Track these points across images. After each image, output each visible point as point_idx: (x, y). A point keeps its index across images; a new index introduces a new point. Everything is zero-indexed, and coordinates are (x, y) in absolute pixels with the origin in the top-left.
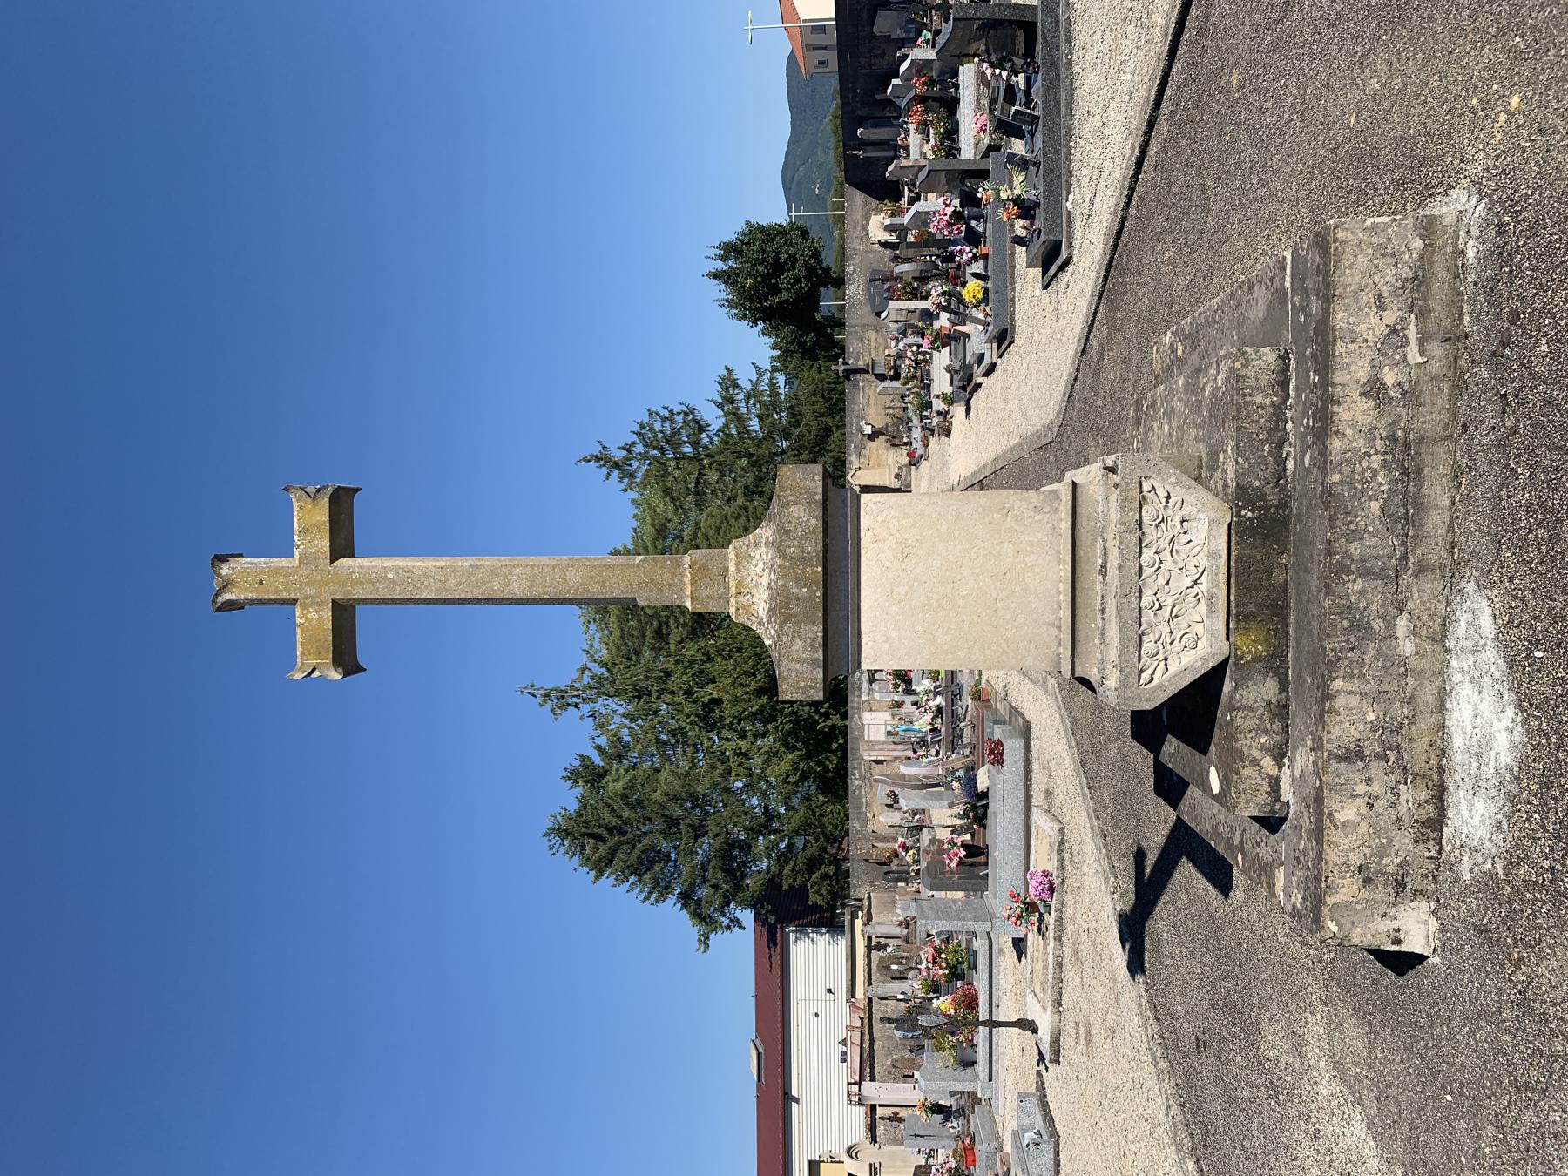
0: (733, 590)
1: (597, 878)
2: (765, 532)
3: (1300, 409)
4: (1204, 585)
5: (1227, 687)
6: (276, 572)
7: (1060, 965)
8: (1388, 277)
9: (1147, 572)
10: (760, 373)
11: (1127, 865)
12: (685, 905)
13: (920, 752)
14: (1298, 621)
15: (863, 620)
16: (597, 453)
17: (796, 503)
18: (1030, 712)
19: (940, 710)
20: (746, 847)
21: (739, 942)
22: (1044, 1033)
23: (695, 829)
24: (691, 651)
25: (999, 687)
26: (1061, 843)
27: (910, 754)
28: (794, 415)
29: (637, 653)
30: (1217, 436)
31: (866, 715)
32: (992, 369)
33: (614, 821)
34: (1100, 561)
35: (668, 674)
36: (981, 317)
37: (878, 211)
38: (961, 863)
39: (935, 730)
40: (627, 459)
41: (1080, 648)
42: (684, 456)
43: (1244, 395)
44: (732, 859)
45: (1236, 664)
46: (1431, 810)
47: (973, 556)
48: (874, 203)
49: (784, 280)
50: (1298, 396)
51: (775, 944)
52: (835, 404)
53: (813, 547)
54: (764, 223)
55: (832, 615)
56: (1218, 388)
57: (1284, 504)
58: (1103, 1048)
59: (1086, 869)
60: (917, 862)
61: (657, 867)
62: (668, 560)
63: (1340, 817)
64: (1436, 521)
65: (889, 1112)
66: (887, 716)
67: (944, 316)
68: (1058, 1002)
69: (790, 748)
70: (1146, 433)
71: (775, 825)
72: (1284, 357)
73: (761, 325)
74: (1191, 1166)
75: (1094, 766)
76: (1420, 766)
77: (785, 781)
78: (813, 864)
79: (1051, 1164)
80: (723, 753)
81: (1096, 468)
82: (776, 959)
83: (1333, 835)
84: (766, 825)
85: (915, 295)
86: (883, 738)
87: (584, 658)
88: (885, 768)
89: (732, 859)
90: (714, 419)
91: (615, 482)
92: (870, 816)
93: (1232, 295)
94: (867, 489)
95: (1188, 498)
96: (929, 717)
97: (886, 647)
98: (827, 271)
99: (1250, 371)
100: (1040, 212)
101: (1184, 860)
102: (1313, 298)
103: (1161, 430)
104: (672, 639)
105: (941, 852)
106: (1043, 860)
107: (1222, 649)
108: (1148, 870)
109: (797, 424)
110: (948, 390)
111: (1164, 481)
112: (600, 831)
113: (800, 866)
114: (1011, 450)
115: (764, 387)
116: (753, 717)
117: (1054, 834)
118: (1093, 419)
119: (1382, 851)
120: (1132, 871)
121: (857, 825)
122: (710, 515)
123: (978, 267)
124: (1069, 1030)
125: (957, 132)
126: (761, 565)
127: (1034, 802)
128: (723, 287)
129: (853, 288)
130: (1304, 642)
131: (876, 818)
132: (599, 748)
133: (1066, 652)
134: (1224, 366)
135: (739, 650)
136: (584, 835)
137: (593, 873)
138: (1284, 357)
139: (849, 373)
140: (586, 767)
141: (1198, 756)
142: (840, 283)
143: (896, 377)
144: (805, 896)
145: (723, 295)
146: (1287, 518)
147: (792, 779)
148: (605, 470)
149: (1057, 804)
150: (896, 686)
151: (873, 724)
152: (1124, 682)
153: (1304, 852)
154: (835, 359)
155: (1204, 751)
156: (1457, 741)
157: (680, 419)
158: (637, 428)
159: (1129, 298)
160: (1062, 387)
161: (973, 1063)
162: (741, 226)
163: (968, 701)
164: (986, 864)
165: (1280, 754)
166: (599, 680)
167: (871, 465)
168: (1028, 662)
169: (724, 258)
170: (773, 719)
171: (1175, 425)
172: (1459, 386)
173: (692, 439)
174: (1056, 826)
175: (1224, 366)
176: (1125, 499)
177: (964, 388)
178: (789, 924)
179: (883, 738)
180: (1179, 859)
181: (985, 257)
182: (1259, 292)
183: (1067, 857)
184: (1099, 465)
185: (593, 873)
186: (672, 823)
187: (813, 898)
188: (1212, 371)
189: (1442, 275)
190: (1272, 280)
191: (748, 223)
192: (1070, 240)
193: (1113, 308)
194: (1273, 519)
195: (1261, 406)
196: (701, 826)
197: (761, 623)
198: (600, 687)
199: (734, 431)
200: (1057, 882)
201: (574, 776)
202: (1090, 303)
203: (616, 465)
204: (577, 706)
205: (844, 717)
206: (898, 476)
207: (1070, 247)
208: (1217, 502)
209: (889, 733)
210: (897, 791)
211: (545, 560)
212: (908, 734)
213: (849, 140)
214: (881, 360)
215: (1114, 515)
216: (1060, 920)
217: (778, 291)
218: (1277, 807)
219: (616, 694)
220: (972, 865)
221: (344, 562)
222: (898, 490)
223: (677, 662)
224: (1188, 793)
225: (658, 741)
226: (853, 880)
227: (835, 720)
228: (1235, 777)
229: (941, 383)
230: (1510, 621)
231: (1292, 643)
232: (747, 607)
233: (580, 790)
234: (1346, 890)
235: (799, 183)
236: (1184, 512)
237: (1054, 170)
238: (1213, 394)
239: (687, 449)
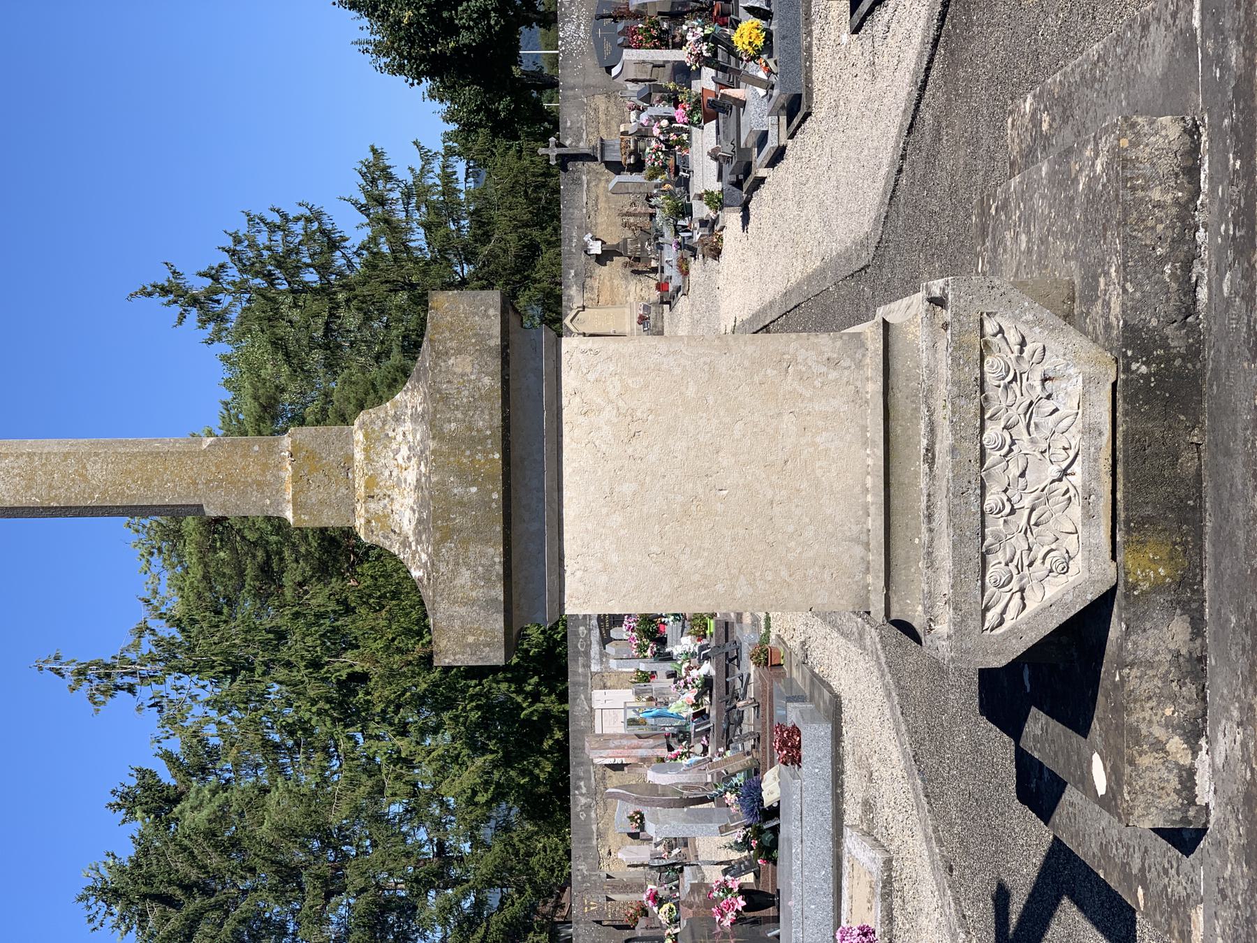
0: (361, 492)
2: (410, 398)
3: (1216, 208)
5: (1115, 630)
9: (993, 457)
10: (427, 157)
13: (678, 750)
14: (1217, 530)
15: (566, 536)
16: (162, 281)
17: (459, 352)
18: (841, 681)
19: (707, 683)
20: (408, 909)
23: (326, 882)
24: (319, 597)
25: (795, 645)
26: (888, 882)
27: (664, 752)
28: (481, 225)
29: (230, 602)
30: (1096, 251)
32: (778, 156)
33: (194, 874)
34: (924, 442)
35: (281, 635)
36: (762, 75)
38: (739, 920)
39: (701, 715)
41: (899, 576)
42: (306, 288)
43: (1134, 189)
45: (1126, 596)
47: (737, 435)
50: (1213, 190)
52: (544, 210)
53: (488, 420)
55: (517, 529)
56: (1096, 179)
57: (1194, 353)
59: (923, 921)
60: (675, 921)
62: (256, 445)
66: (627, 695)
67: (708, 72)
70: (994, 250)
71: (455, 872)
72: (1192, 131)
73: (426, 84)
75: (933, 762)
77: (471, 801)
80: (371, 759)
81: (918, 300)
84: (442, 870)
85: (664, 40)
86: (621, 729)
87: (144, 612)
88: (627, 777)
90: (354, 229)
92: (604, 852)
93: (1119, 39)
95: (1052, 346)
96: (690, 695)
97: (604, 578)
99: (1143, 153)
101: (1065, 901)
102: (1232, 42)
103: (1017, 242)
104: (288, 580)
105: (710, 902)
107: (1105, 574)
108: (1014, 919)
109: (485, 238)
110: (716, 187)
111: (1016, 318)
112: (171, 890)
114: (809, 279)
115: (433, 180)
116: (420, 701)
117: (876, 868)
118: (927, 224)
120: (991, 921)
121: (583, 867)
122: (348, 382)
126: (405, 451)
127: (848, 819)
128: (365, 21)
130: (1226, 562)
132: (169, 757)
134: (1104, 145)
135: (395, 595)
136: (144, 897)
138: (1192, 131)
139: (565, 160)
140: (147, 788)
141: (1076, 738)
143: (638, 166)
145: (366, 35)
146: (1199, 374)
147: (481, 798)
148: (176, 309)
149: (880, 821)
150: (642, 649)
151: (607, 707)
152: (960, 626)
153: (1232, 880)
154: (544, 138)
155: (1084, 730)
157: (298, 228)
158: (229, 243)
159: (975, 46)
160: (880, 184)
163: (750, 668)
164: (777, 919)
165: (1194, 733)
168: (822, 599)
170: (449, 704)
171: (1036, 235)
173: (319, 260)
174: (880, 857)
175: (1104, 145)
176: (958, 346)
177: (738, 184)
179: (621, 729)
180: (1058, 900)
182: (1157, 34)
183: (897, 903)
184: (921, 295)
186: (289, 875)
188: (1088, 153)
190: (1174, 16)
193: (954, 61)
194: (1179, 375)
195: (1159, 205)
196: (335, 877)
197: (405, 544)
199: (385, 249)
201: (127, 802)
202: (920, 54)
203: (195, 301)
204: (131, 689)
205: (563, 697)
208: (1094, 350)
209: (632, 722)
210: (646, 811)
211: (52, 445)
212: (662, 722)
214: (614, 140)
215: (944, 371)
217: (451, 30)
218: (1191, 813)
219: (197, 669)
220: (756, 922)
223: (296, 615)
224: (1066, 797)
225: (266, 743)
227: (549, 702)
228: (1128, 769)
229: (706, 177)
231: (1209, 563)
232: (383, 518)
233: (139, 825)
236: (1046, 365)
238: (1089, 187)
239: (311, 277)
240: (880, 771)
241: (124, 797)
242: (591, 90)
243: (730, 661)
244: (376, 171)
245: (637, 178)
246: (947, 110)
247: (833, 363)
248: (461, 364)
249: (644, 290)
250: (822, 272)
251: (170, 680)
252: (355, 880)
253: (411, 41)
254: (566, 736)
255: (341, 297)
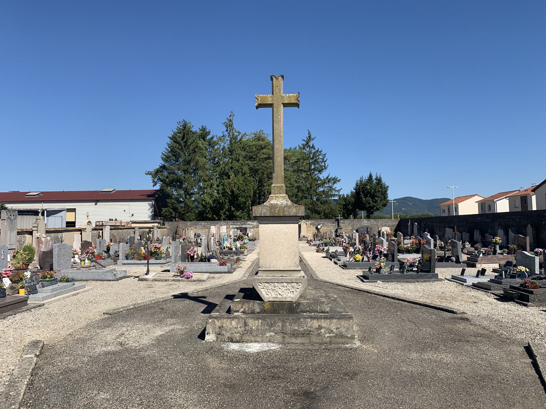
1: (170, 138)
2: (290, 203)
4: (279, 296)
6: (280, 90)
7: (166, 281)
8: (343, 330)
10: (338, 191)
11: (200, 294)
12: (161, 167)
19: (232, 249)
20: (180, 187)
21: (148, 185)
22: (146, 277)
23: (187, 170)
24: (246, 169)
25: (241, 265)
26: (201, 281)
27: (217, 240)
31: (225, 227)
32: (336, 263)
33: (189, 143)
35: (238, 161)
37: (391, 230)
40: (309, 146)
41: (265, 272)
42: (310, 166)
44: (177, 183)
46: (235, 340)
48: (394, 228)
49: (369, 199)
51: (148, 197)
52: (327, 216)
53: (287, 214)
54: (388, 192)
57: (297, 313)
58: (148, 290)
61: (173, 158)
63: (233, 322)
64: (293, 340)
65: (101, 234)
67: (353, 250)
68: (156, 280)
69: (214, 202)
73: (354, 191)
74: (132, 307)
76: (244, 338)
77: (203, 200)
78: (175, 209)
79: (109, 279)
82: (143, 197)
83: (229, 321)
87: (243, 133)
89: (177, 183)
90: (323, 176)
91: (302, 143)
94: (300, 226)
96: (229, 246)
98: (372, 213)
99: (324, 305)
100: (377, 274)
104: (249, 162)
106: (196, 276)
107: (266, 300)
109: (322, 204)
110: (330, 251)
113: (175, 205)
115: (334, 192)
116: (224, 189)
119: (226, 330)
123: (366, 259)
124: (149, 283)
125: (409, 253)
128: (367, 178)
129: (366, 222)
131: (190, 230)
132: (213, 138)
133: (264, 269)
135: (246, 185)
136: (184, 133)
137: (171, 136)
139: (338, 220)
140: (206, 133)
142: (368, 217)
143: (337, 236)
144: (165, 206)
145: (364, 178)
147: (203, 202)
148: (306, 139)
156: (249, 344)
157: (323, 164)
158: (320, 150)
159: (350, 294)
161: (127, 259)
162: (387, 184)
163: (236, 257)
165: (244, 312)
166: (235, 138)
167: (308, 228)
169: (376, 179)
170: (223, 196)
172: (321, 344)
174: (205, 279)
177: (331, 256)
178: (155, 201)
181: (369, 261)
185: (171, 136)
186: (188, 163)
187: (164, 210)
189: (343, 341)
191: (388, 187)
192: (369, 282)
198: (233, 139)
199: (319, 182)
200: (190, 279)
201: (203, 129)
203: (307, 143)
204: (227, 130)
205: (224, 220)
206: (304, 237)
207: (367, 282)
213: (413, 220)
216: (179, 280)
219: (231, 144)
221: (282, 106)
222: (299, 237)
226: (171, 223)
229: (332, 249)
230: (274, 351)
234: (218, 323)
235: (406, 203)
237: (387, 279)
239: (313, 167)
240: (220, 280)
241: (205, 129)
242: (353, 226)
243: (236, 254)
244: (335, 180)
245: (334, 236)
246: (340, 290)
247: (295, 263)
248: (294, 210)
249: (310, 237)
250: (313, 270)
251: (229, 138)
252: (187, 176)
253: (363, 188)
254: (216, 220)
255: (308, 173)
